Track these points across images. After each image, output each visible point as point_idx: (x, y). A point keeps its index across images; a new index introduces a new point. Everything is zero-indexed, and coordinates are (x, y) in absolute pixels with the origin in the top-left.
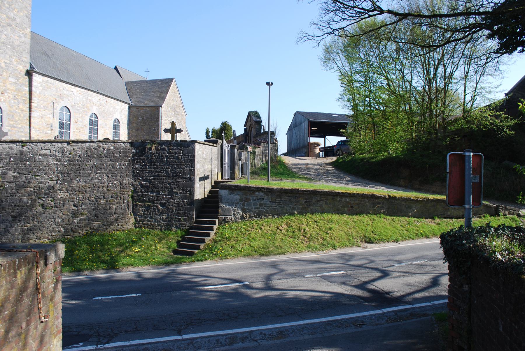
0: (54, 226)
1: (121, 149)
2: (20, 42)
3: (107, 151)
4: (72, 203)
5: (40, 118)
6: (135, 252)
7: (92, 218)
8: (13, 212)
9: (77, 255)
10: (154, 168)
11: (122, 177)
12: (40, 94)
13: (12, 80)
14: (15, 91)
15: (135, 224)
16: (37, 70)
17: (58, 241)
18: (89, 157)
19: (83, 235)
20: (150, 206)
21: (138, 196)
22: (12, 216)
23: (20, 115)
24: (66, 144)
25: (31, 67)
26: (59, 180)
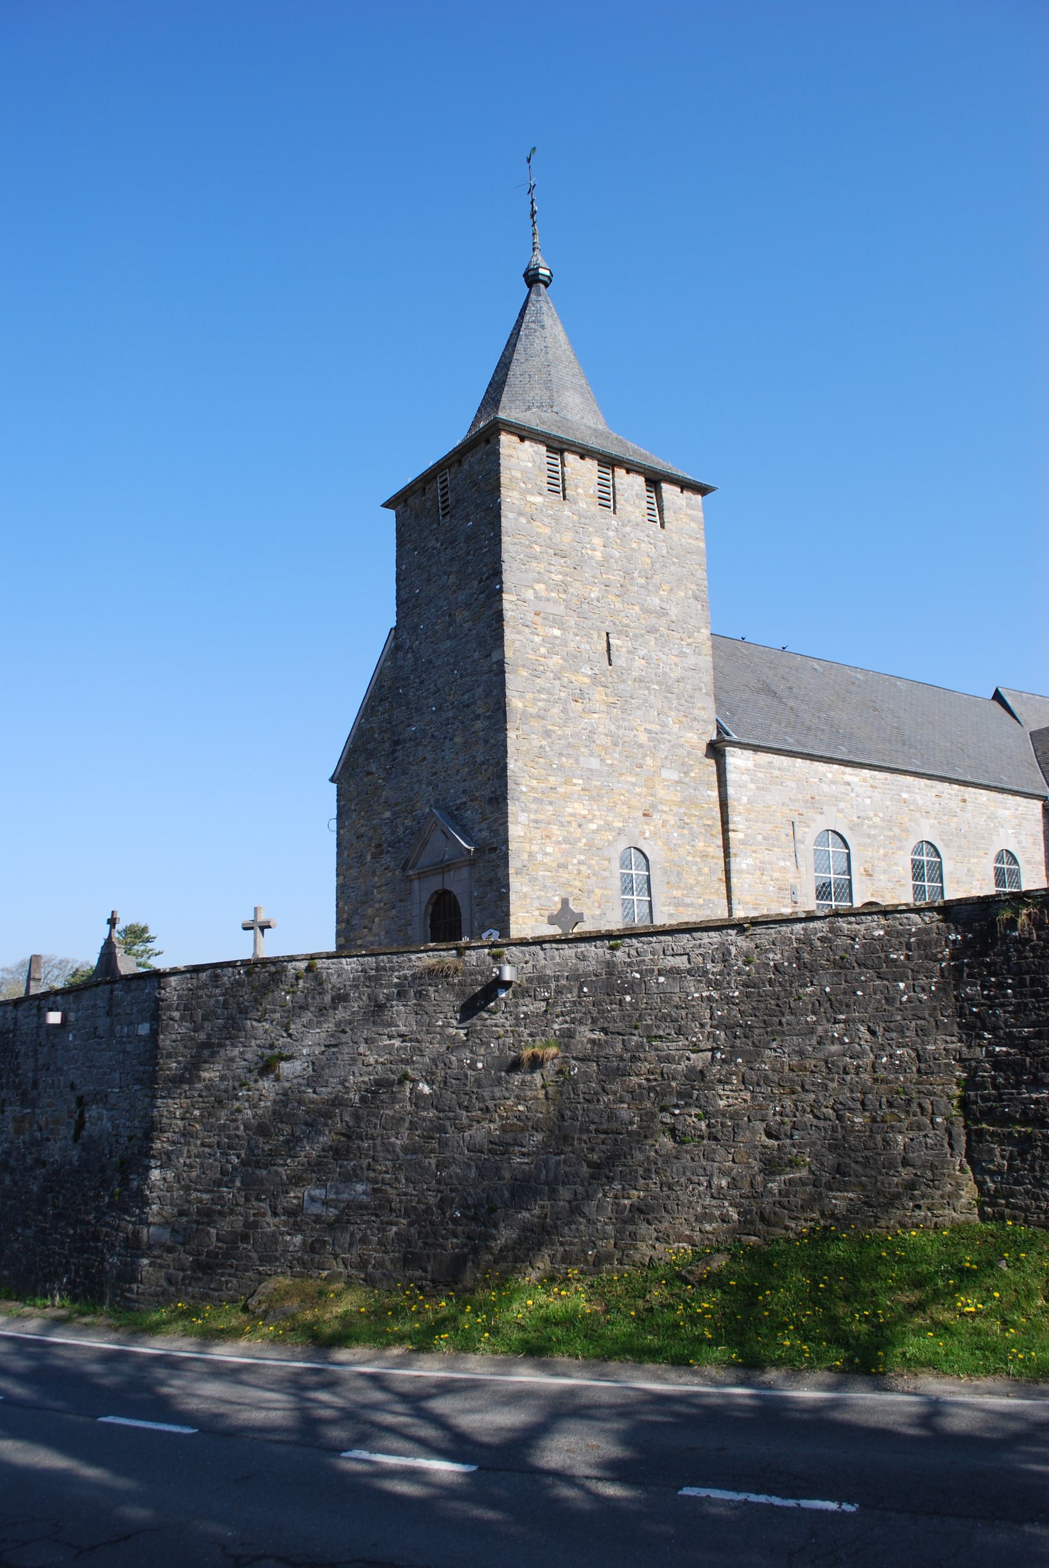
0: (708, 1201)
1: (911, 935)
2: (683, 668)
3: (863, 946)
4: (760, 1126)
5: (758, 873)
6: (962, 1314)
7: (826, 1177)
8: (592, 1150)
9: (765, 1307)
10: (1035, 995)
11: (922, 1032)
12: (750, 802)
13: (670, 774)
14: (680, 804)
15: (981, 1205)
16: (735, 737)
17: (718, 1251)
18: (807, 969)
19: (800, 1235)
20: (1028, 1138)
21: (985, 1099)
22: (591, 1164)
23: (699, 871)
24: (733, 932)
25: (719, 733)
26: (718, 1049)
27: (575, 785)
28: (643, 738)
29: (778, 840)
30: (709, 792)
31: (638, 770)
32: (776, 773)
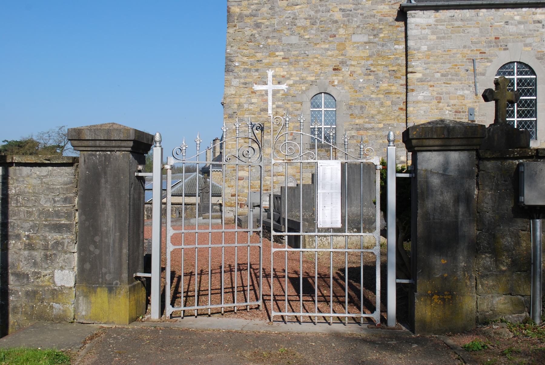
5: (435, 102)
23: (382, 105)
27: (277, 56)
28: (338, 16)
29: (457, 75)
30: (396, 46)
31: (332, 39)
32: (460, 23)
